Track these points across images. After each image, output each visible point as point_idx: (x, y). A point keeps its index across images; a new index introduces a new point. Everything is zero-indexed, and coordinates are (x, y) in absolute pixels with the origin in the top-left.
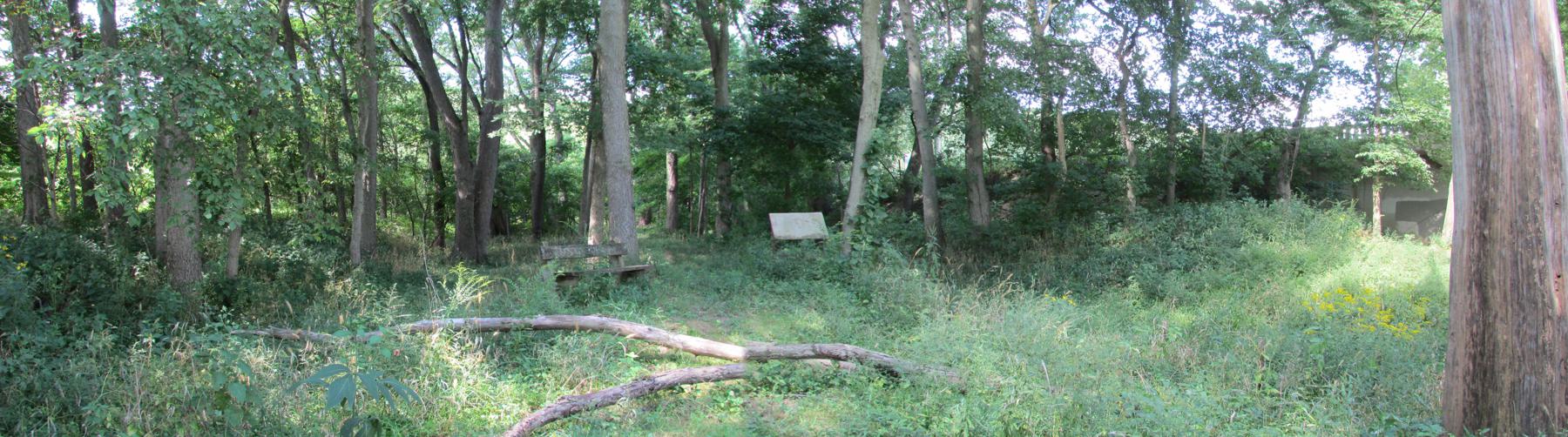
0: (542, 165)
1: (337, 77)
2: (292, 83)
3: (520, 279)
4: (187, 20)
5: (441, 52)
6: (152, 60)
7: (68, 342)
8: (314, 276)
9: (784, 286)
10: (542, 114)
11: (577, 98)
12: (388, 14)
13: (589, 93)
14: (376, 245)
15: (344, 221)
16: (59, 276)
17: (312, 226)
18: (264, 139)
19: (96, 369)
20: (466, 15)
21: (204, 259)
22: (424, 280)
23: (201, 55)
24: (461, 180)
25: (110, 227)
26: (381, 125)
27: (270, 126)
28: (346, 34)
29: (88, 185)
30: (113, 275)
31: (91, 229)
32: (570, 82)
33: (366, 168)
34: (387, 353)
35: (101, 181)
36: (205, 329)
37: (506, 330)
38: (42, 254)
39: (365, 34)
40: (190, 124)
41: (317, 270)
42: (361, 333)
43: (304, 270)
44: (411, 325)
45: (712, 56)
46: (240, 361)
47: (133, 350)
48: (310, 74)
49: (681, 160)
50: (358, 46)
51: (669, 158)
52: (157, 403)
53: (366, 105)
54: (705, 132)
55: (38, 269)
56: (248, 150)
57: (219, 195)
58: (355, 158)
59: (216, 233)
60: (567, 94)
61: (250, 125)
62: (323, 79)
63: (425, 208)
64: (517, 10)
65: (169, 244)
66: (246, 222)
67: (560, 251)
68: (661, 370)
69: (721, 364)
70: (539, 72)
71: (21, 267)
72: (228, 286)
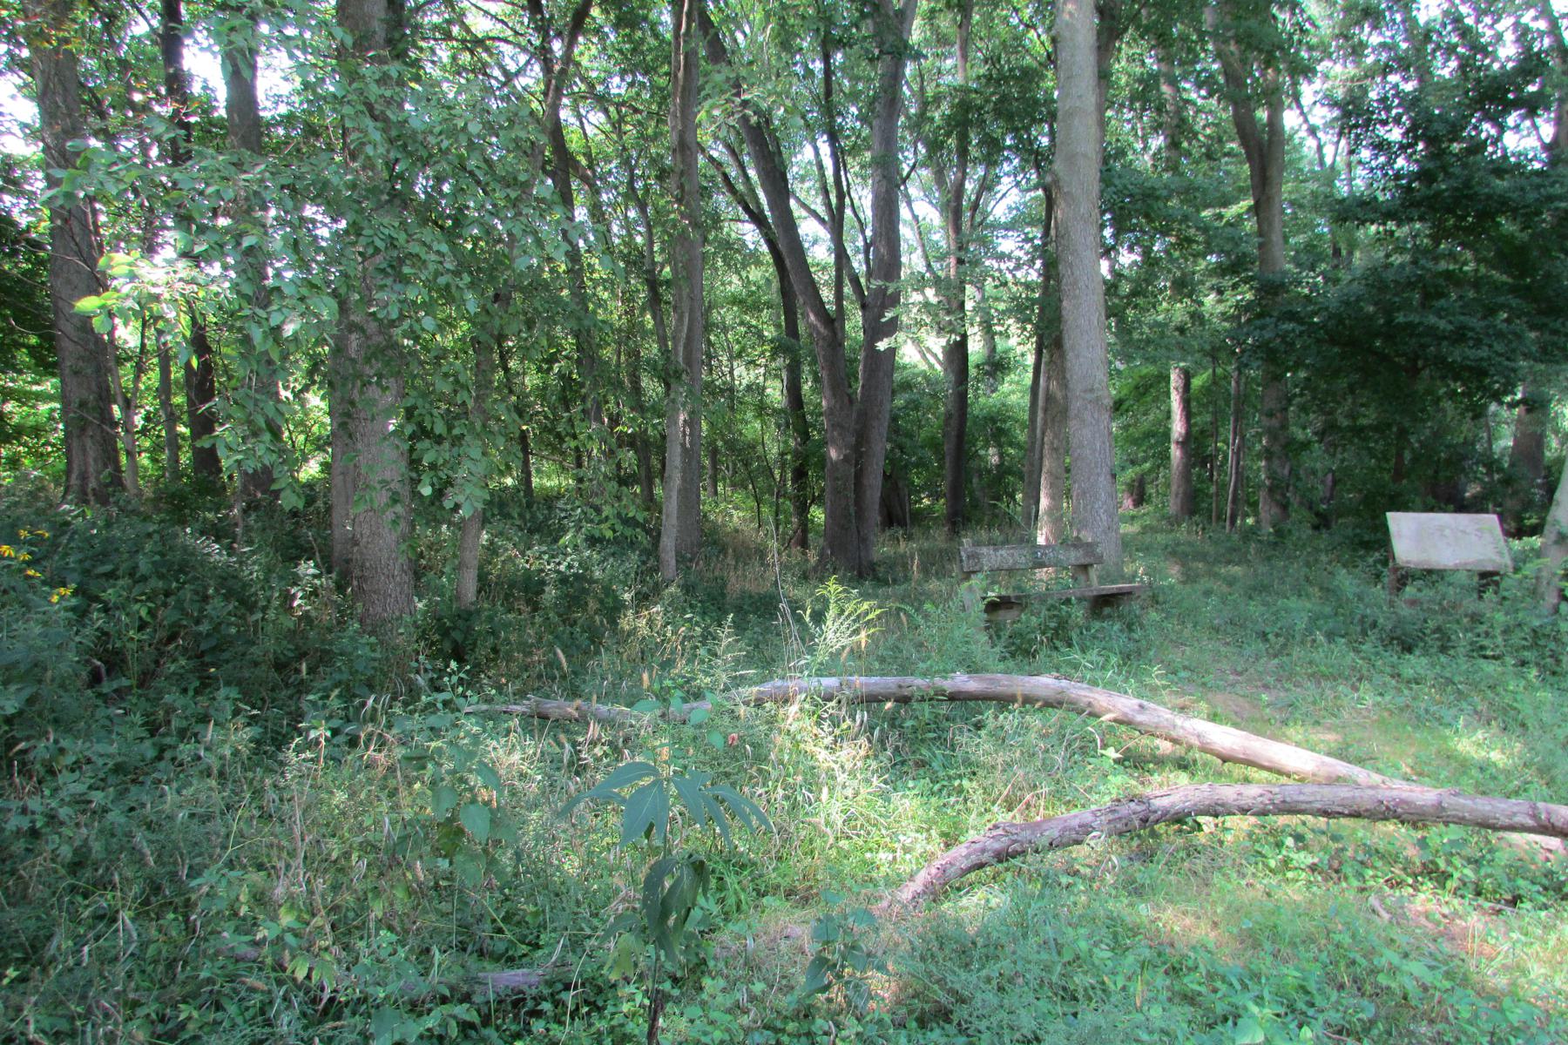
0: (962, 398)
1: (639, 240)
2: (565, 247)
3: (928, 606)
4: (388, 113)
5: (802, 196)
6: (326, 184)
7: (162, 750)
8: (601, 601)
9: (1414, 664)
10: (962, 305)
11: (1019, 274)
12: (719, 127)
13: (1038, 264)
14: (700, 545)
15: (650, 502)
16: (143, 613)
17: (598, 510)
18: (520, 348)
19: (218, 799)
20: (841, 129)
21: (418, 573)
22: (776, 608)
23: (413, 184)
24: (834, 426)
25: (245, 512)
26: (708, 327)
27: (530, 324)
28: (654, 161)
29: (204, 425)
30: (251, 608)
31: (210, 515)
32: (1008, 244)
33: (684, 405)
34: (717, 740)
35: (229, 417)
36: (420, 705)
37: (904, 700)
38: (108, 568)
39: (683, 162)
40: (394, 316)
41: (607, 590)
42: (676, 706)
43: (585, 591)
44: (755, 689)
45: (1252, 177)
46: (480, 762)
47: (291, 754)
48: (595, 231)
49: (1196, 382)
50: (671, 183)
51: (1175, 379)
52: (334, 855)
53: (685, 292)
54: (1239, 324)
55: (97, 599)
56: (494, 369)
57: (443, 453)
58: (668, 386)
59: (439, 523)
60: (1003, 266)
61: (497, 322)
62: (617, 241)
63: (778, 477)
64: (922, 117)
65: (356, 544)
66: (489, 503)
67: (992, 557)
68: (1161, 785)
69: (1269, 782)
70: (957, 229)
71: (61, 597)
72: (460, 623)
